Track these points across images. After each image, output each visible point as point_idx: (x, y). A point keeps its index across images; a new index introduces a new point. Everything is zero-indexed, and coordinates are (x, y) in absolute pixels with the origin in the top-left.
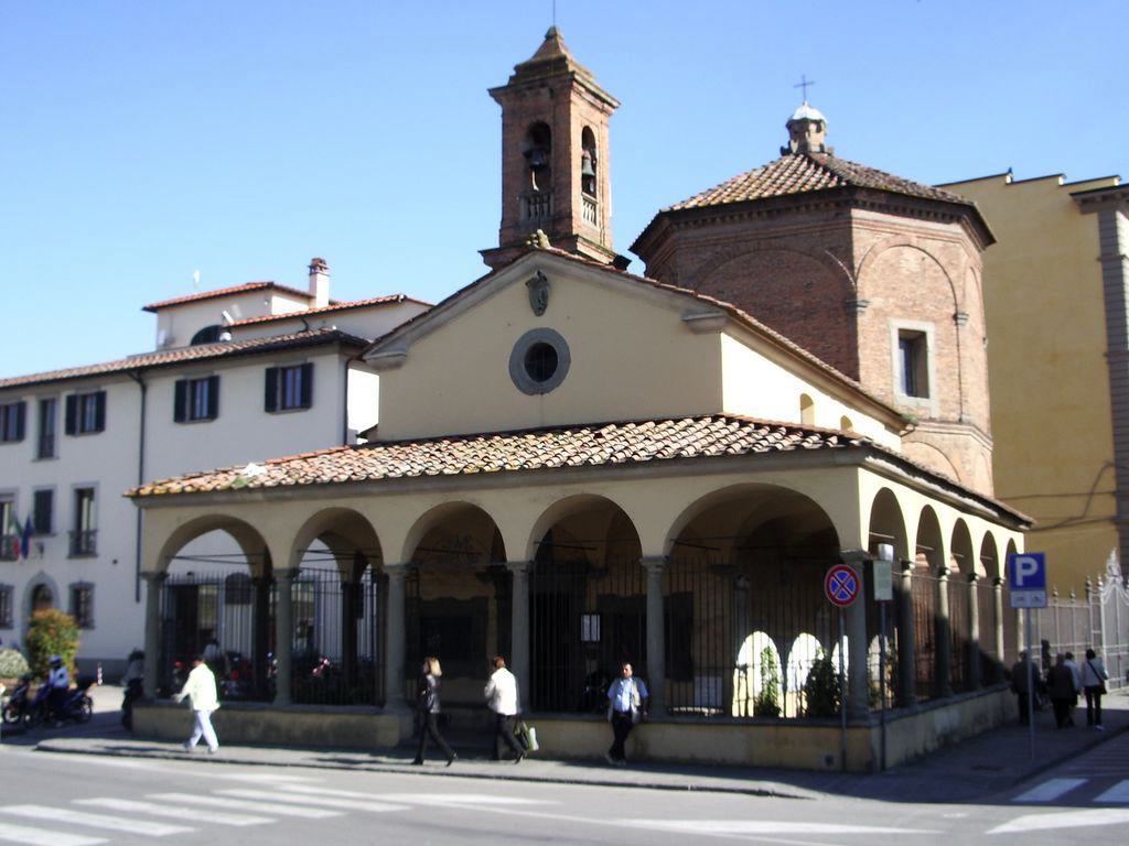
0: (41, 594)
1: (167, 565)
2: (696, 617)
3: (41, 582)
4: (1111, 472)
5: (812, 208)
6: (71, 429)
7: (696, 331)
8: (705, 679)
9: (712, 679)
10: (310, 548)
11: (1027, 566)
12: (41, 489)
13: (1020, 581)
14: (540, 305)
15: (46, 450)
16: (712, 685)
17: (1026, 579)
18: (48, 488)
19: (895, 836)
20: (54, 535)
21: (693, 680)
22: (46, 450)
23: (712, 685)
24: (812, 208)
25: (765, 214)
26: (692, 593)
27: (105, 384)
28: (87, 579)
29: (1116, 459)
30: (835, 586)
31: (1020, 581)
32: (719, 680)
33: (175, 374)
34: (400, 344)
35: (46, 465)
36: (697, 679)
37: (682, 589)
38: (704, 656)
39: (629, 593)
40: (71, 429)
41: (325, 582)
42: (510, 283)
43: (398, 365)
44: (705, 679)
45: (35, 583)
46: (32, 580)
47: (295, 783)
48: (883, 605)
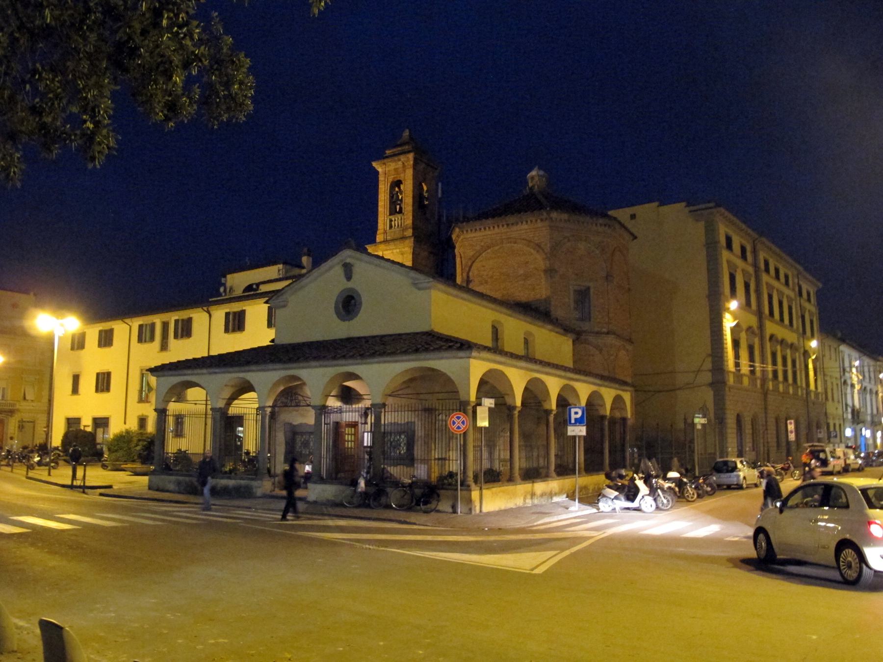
1: (326, 401)
2: (416, 434)
4: (710, 359)
5: (529, 222)
6: (176, 337)
7: (419, 289)
8: (419, 465)
9: (423, 466)
10: (331, 394)
11: (576, 413)
13: (573, 421)
14: (349, 277)
15: (164, 347)
16: (423, 468)
17: (576, 419)
20: (80, 395)
21: (414, 466)
22: (164, 347)
23: (423, 468)
24: (529, 222)
25: (505, 226)
26: (414, 422)
27: (192, 313)
29: (713, 353)
30: (454, 423)
31: (573, 421)
32: (426, 466)
34: (284, 297)
35: (164, 354)
36: (416, 465)
37: (410, 420)
38: (419, 453)
39: (403, 422)
40: (176, 337)
41: (395, 411)
43: (284, 306)
44: (419, 465)
47: (185, 512)
48: (483, 429)
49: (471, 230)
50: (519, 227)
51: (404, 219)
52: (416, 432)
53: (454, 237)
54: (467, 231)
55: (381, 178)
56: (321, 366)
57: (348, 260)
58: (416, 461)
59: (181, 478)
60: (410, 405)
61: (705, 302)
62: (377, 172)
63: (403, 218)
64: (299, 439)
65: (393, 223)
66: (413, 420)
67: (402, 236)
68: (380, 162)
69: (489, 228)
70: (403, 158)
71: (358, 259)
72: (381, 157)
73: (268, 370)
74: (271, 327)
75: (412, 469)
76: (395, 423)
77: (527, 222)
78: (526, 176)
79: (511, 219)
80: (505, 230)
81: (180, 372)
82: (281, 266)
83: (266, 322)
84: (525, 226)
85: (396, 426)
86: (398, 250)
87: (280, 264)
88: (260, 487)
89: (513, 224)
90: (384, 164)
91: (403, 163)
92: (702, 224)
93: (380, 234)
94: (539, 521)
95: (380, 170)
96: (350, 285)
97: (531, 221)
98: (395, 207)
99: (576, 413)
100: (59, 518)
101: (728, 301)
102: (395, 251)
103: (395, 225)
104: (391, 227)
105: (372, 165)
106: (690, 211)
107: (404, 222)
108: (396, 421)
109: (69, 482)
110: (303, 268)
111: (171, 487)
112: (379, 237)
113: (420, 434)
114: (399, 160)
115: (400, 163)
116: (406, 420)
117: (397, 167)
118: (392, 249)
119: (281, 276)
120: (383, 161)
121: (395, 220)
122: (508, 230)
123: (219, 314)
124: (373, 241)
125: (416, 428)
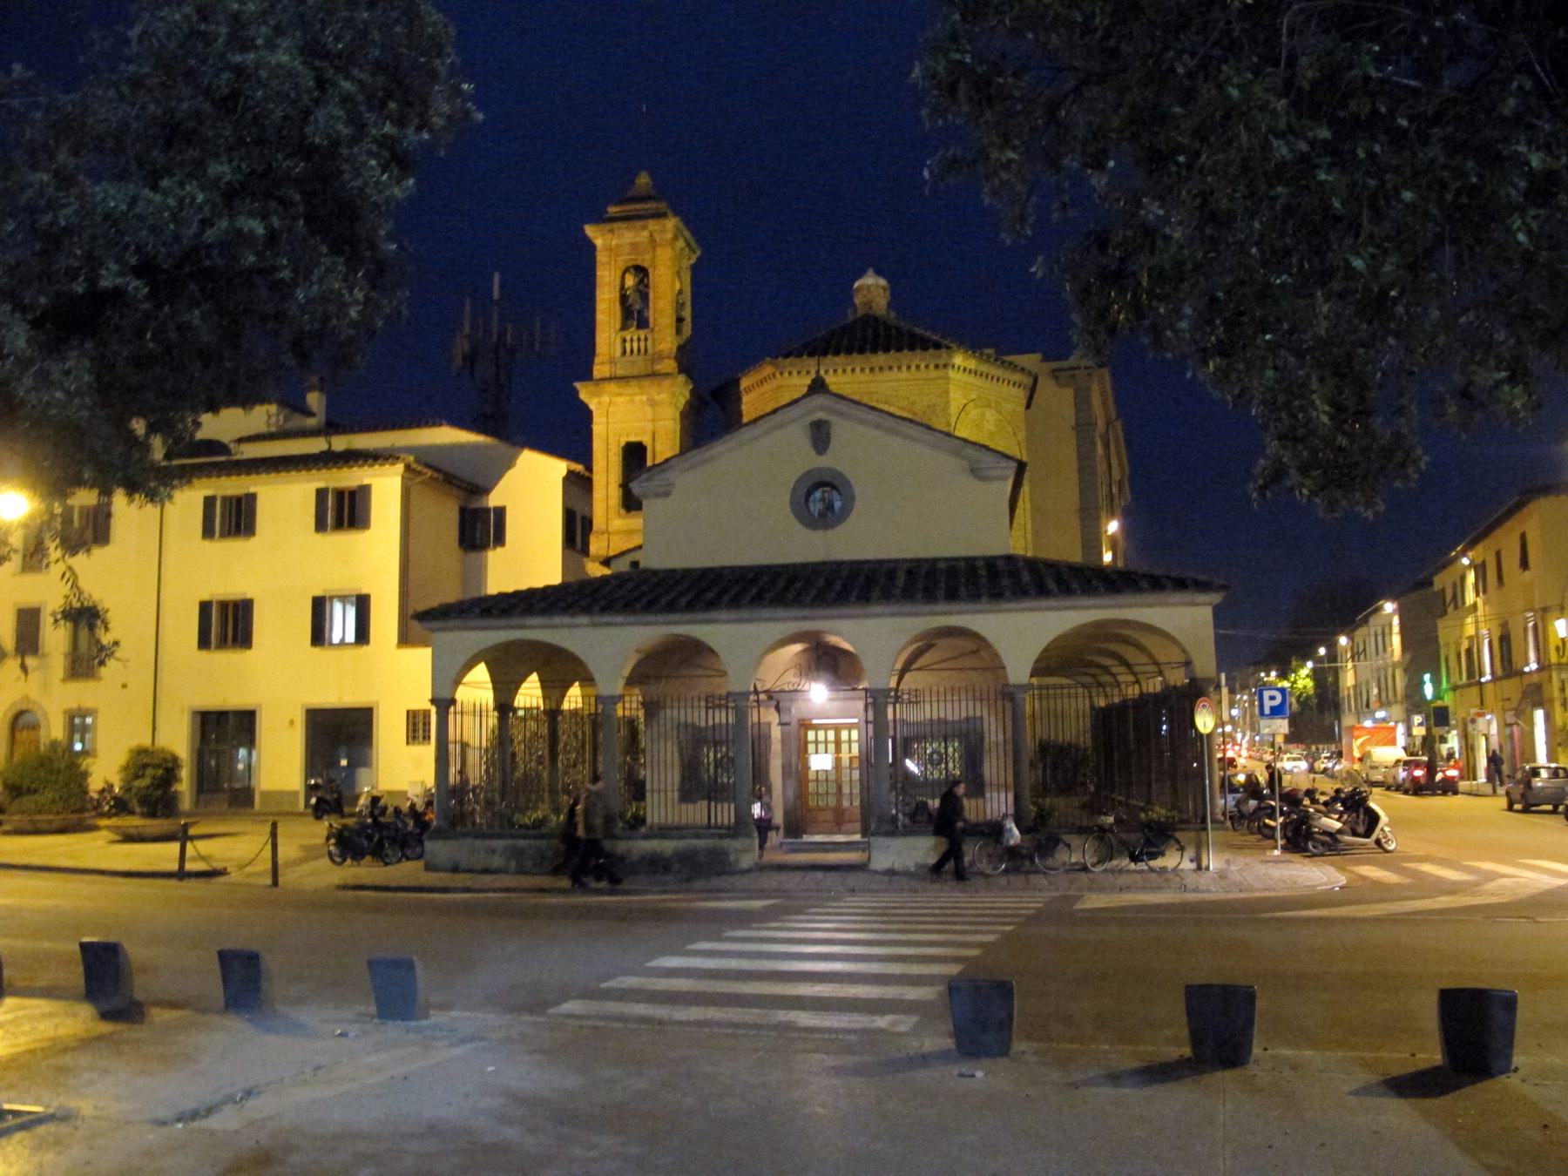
0: (22, 721)
3: (24, 707)
5: (913, 367)
11: (1272, 698)
12: (26, 606)
13: (1267, 711)
16: (656, 815)
18: (36, 605)
19: (1287, 910)
23: (656, 815)
26: (982, 718)
27: (256, 485)
28: (88, 703)
31: (1267, 711)
32: (732, 806)
33: (205, 487)
36: (988, 795)
37: (971, 713)
39: (956, 717)
42: (792, 421)
43: (667, 494)
45: (19, 708)
46: (14, 704)
49: (799, 373)
50: (895, 374)
51: (654, 340)
52: (987, 735)
53: (745, 383)
54: (790, 373)
55: (601, 257)
56: (893, 615)
57: (820, 415)
58: (987, 788)
59: (522, 843)
60: (935, 689)
61: (1075, 522)
62: (593, 247)
63: (650, 337)
64: (709, 756)
65: (628, 346)
66: (978, 714)
67: (649, 371)
68: (601, 226)
69: (835, 371)
70: (652, 225)
71: (841, 414)
72: (601, 218)
73: (760, 620)
74: (325, 530)
75: (980, 801)
76: (939, 719)
77: (909, 367)
78: (853, 281)
79: (880, 359)
80: (866, 378)
81: (511, 622)
82: (273, 408)
83: (312, 521)
84: (904, 374)
85: (943, 726)
86: (644, 398)
87: (270, 403)
88: (747, 852)
89: (881, 369)
90: (612, 231)
91: (651, 235)
92: (1068, 393)
93: (602, 363)
94: (764, 907)
95: (599, 242)
96: (824, 462)
97: (918, 367)
98: (634, 313)
99: (1272, 698)
100: (1468, 866)
101: (1107, 523)
102: (637, 398)
103: (632, 351)
104: (624, 352)
105: (583, 231)
106: (1054, 371)
107: (654, 345)
108: (942, 715)
109: (174, 867)
110: (311, 414)
111: (497, 862)
112: (599, 370)
113: (993, 738)
114: (644, 228)
115: (646, 233)
116: (964, 714)
117: (637, 240)
118: (632, 395)
119: (273, 429)
120: (609, 226)
121: (632, 340)
122: (871, 377)
123: (188, 502)
124: (587, 375)
125: (986, 727)
